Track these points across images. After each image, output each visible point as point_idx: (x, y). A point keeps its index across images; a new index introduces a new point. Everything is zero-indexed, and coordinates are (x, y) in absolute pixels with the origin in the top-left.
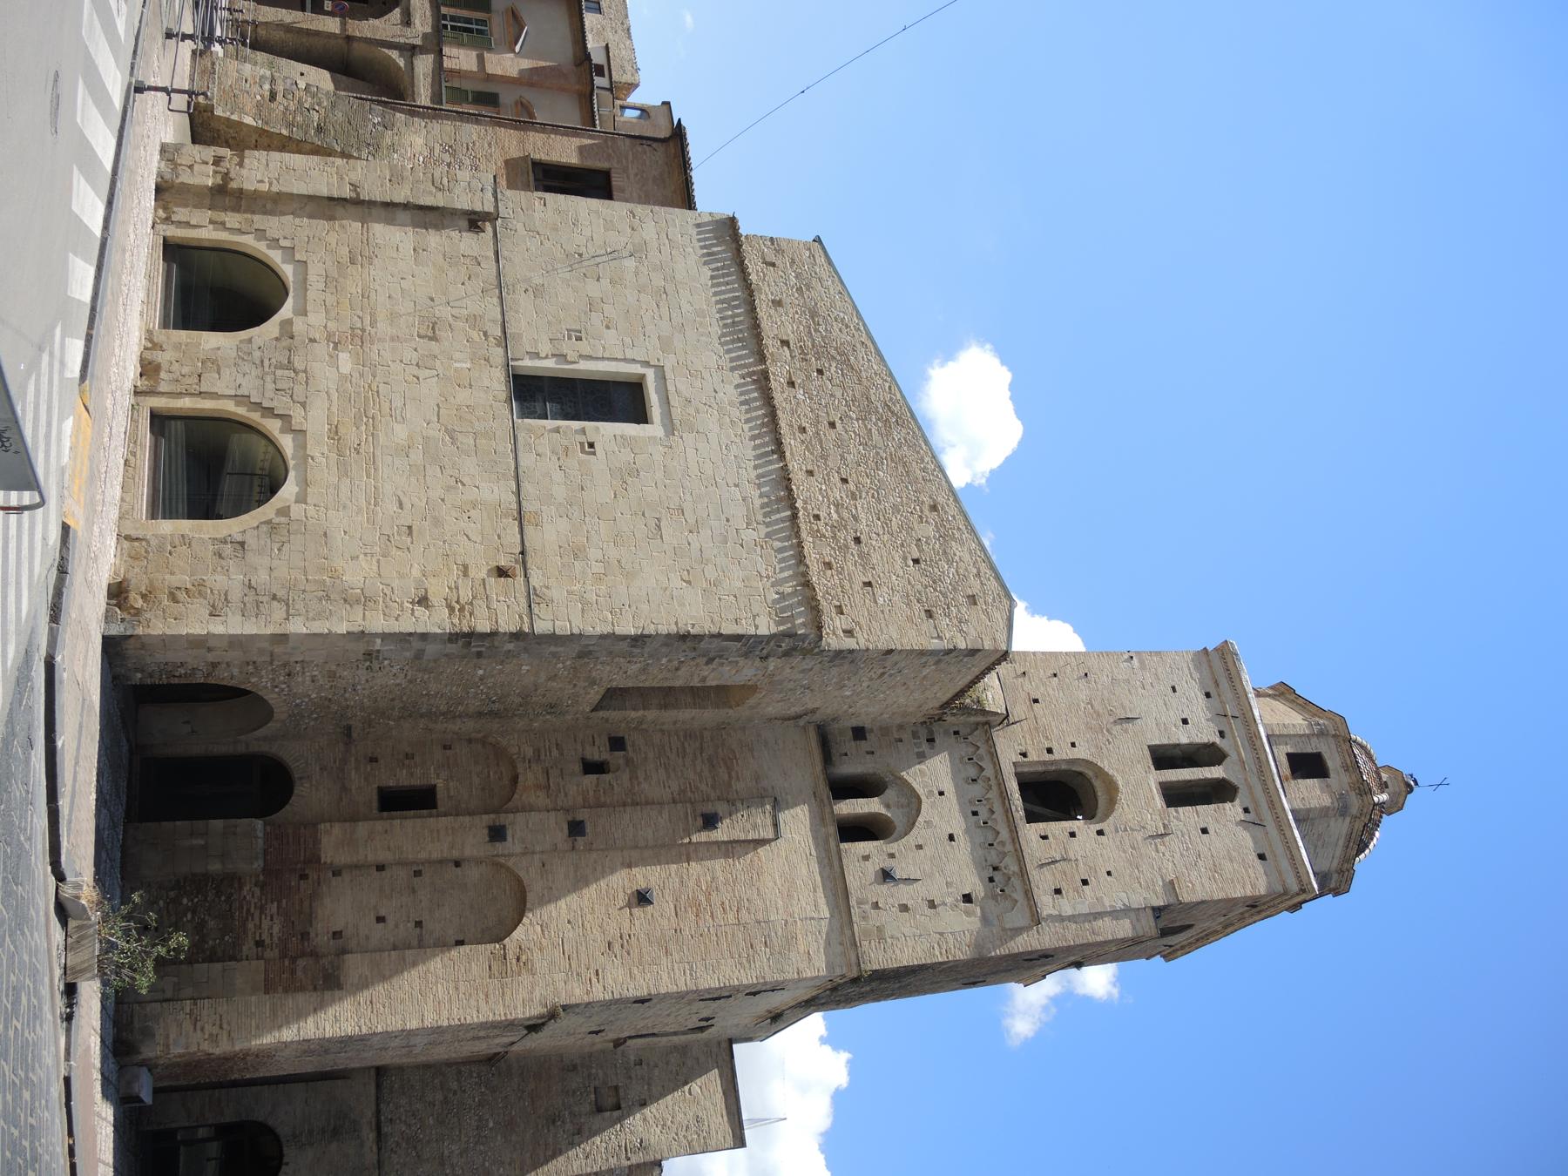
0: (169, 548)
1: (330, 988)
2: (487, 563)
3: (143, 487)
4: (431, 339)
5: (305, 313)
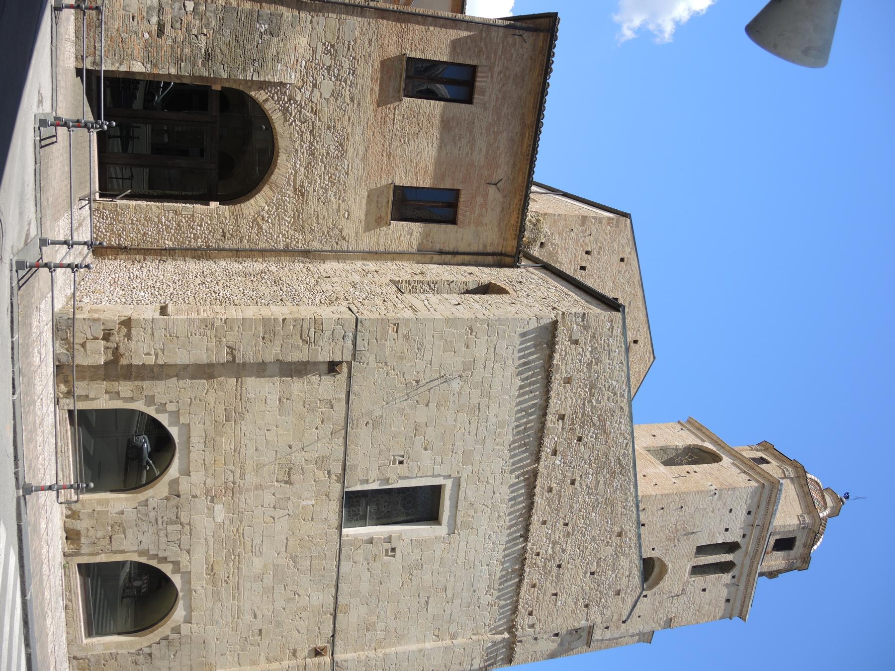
0: (103, 662)
2: (309, 646)
3: (80, 622)
4: (286, 482)
5: (188, 474)
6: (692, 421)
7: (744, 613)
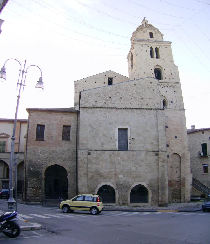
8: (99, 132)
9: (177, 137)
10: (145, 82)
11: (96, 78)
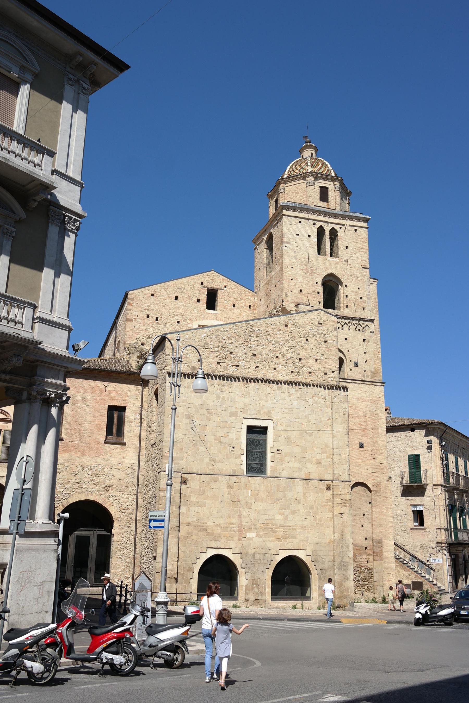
1: (382, 542)
6: (254, 241)
7: (366, 219)
8: (206, 433)
9: (364, 445)
10: (309, 319)
11: (178, 288)
